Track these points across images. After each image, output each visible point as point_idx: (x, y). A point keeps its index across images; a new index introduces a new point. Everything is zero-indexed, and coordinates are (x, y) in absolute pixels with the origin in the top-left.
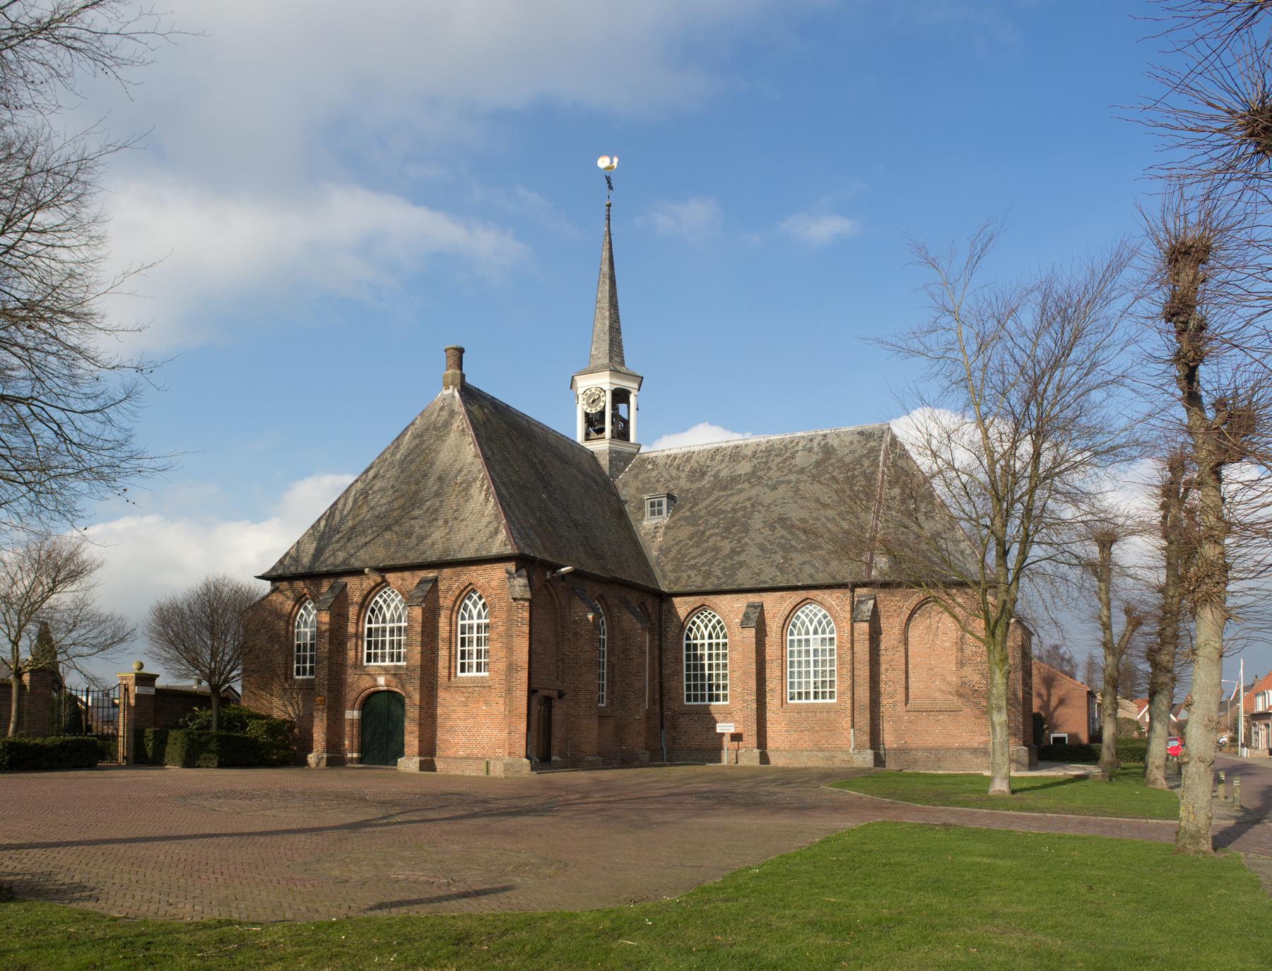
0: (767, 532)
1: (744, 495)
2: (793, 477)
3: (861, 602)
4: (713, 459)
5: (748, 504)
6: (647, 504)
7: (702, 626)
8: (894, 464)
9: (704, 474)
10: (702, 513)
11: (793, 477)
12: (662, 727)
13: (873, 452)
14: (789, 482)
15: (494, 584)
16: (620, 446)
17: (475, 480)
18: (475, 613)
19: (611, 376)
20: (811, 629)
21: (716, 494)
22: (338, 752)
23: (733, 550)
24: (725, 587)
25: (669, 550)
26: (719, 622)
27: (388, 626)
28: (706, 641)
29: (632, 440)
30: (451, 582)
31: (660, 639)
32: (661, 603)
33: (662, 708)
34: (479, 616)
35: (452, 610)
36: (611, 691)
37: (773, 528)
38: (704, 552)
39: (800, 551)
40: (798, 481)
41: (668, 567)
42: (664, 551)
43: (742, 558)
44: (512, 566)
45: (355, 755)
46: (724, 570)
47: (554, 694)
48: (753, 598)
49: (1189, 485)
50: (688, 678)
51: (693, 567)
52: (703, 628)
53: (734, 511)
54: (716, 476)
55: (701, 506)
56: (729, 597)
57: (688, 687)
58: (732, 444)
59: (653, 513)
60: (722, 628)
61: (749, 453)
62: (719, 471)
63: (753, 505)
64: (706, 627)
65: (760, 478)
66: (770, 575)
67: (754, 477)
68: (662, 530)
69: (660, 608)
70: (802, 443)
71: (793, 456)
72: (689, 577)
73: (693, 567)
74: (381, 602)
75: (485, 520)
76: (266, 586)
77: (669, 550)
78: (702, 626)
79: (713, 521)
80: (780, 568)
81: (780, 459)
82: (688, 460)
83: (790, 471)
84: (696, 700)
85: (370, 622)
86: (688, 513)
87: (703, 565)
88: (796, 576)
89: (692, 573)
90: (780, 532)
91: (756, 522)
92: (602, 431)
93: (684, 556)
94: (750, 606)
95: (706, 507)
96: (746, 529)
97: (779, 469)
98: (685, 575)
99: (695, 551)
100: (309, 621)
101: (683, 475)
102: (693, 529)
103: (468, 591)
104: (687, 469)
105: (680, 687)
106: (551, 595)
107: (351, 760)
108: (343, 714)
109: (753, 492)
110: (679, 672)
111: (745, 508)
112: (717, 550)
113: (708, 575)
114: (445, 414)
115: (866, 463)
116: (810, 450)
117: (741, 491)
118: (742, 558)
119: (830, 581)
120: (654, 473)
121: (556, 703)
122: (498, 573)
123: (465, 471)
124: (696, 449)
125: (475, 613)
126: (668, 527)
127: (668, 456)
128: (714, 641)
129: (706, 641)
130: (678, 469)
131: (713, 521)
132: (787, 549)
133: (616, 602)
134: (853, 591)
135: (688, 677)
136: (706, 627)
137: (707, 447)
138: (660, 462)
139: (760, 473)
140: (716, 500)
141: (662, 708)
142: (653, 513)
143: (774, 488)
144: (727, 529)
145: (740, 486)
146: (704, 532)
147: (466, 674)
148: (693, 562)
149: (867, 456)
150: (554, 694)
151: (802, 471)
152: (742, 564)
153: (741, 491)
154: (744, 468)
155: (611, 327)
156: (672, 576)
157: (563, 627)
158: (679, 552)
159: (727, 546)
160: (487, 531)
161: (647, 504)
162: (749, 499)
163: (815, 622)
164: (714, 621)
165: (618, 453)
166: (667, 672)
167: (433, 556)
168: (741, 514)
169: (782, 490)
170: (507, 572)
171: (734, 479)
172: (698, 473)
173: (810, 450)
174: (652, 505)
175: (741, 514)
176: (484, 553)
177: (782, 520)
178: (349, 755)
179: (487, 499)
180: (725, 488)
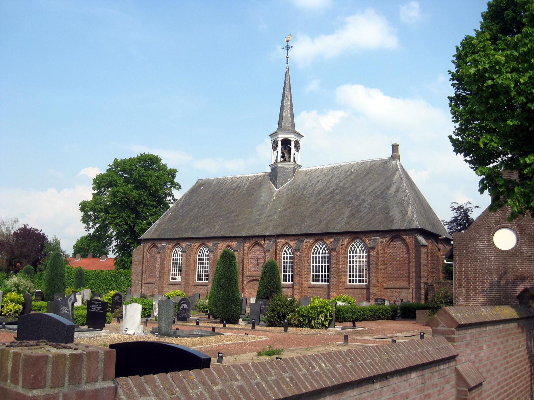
7: (356, 247)
18: (288, 253)
28: (321, 255)
34: (290, 254)
52: (319, 249)
64: (321, 248)
74: (318, 246)
78: (356, 247)
125: (288, 253)
136: (321, 248)
163: (360, 248)
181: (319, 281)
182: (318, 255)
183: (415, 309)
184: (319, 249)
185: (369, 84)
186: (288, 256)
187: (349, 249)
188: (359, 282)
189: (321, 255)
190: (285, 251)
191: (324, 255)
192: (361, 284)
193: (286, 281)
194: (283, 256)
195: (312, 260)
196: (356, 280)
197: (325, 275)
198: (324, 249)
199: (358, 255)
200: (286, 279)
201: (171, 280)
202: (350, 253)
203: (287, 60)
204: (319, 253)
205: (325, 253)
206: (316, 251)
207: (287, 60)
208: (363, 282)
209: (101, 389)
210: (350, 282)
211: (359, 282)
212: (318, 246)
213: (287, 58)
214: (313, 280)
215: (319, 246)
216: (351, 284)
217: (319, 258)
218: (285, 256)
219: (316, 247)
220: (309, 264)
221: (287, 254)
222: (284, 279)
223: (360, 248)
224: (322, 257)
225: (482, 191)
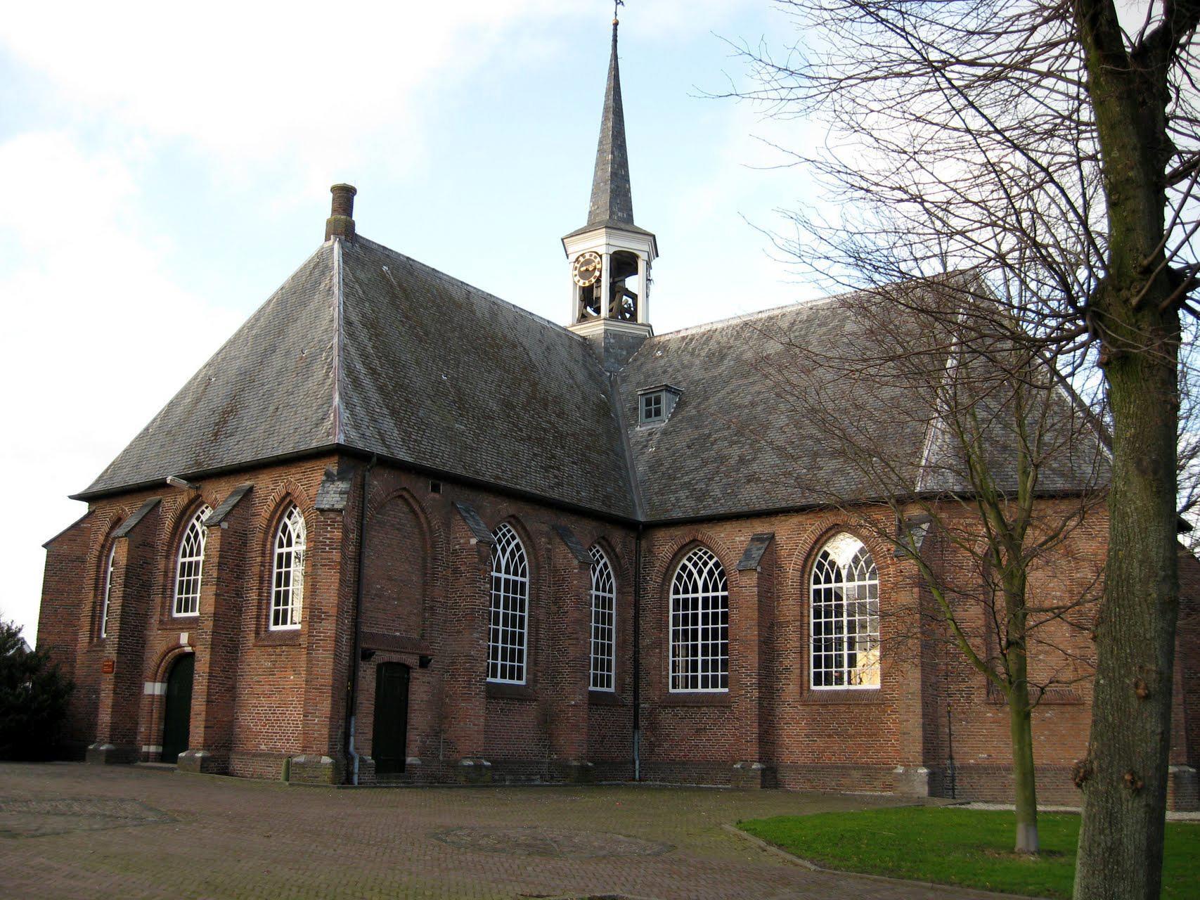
7: (695, 571)
12: (636, 726)
16: (621, 327)
18: (700, 584)
19: (608, 235)
22: (132, 742)
23: (742, 460)
26: (717, 565)
30: (268, 487)
31: (637, 593)
32: (638, 538)
33: (636, 696)
35: (266, 533)
36: (534, 662)
37: (798, 425)
38: (705, 463)
42: (655, 465)
44: (332, 465)
45: (153, 749)
48: (761, 527)
52: (696, 575)
53: (753, 404)
55: (711, 401)
58: (764, 315)
59: (648, 415)
60: (722, 575)
61: (785, 325)
62: (742, 353)
64: (700, 572)
69: (638, 546)
72: (678, 499)
74: (690, 566)
78: (695, 571)
82: (371, 325)
84: (828, 682)
86: (694, 412)
94: (757, 539)
99: (692, 463)
101: (698, 362)
103: (286, 504)
106: (413, 511)
107: (147, 757)
108: (141, 687)
121: (416, 674)
122: (316, 473)
124: (720, 326)
125: (700, 584)
127: (684, 338)
130: (692, 354)
133: (545, 528)
136: (700, 572)
137: (734, 322)
138: (673, 346)
141: (636, 696)
142: (648, 415)
144: (739, 433)
146: (710, 435)
147: (280, 628)
148: (686, 479)
150: (412, 660)
155: (614, 174)
157: (435, 559)
159: (735, 452)
163: (705, 574)
164: (711, 564)
165: (616, 336)
166: (645, 642)
172: (720, 355)
174: (648, 403)
178: (145, 749)
182: (690, 596)
184: (696, 575)
187: (674, 580)
188: (705, 685)
189: (700, 595)
191: (711, 594)
193: (695, 686)
195: (671, 628)
197: (715, 662)
199: (700, 595)
200: (695, 678)
202: (677, 592)
203: (615, 30)
207: (615, 30)
211: (705, 685)
212: (690, 566)
213: (616, 24)
215: (695, 565)
216: (823, 688)
217: (695, 607)
219: (684, 568)
220: (662, 626)
222: (818, 675)
223: (705, 574)
225: (44, 546)
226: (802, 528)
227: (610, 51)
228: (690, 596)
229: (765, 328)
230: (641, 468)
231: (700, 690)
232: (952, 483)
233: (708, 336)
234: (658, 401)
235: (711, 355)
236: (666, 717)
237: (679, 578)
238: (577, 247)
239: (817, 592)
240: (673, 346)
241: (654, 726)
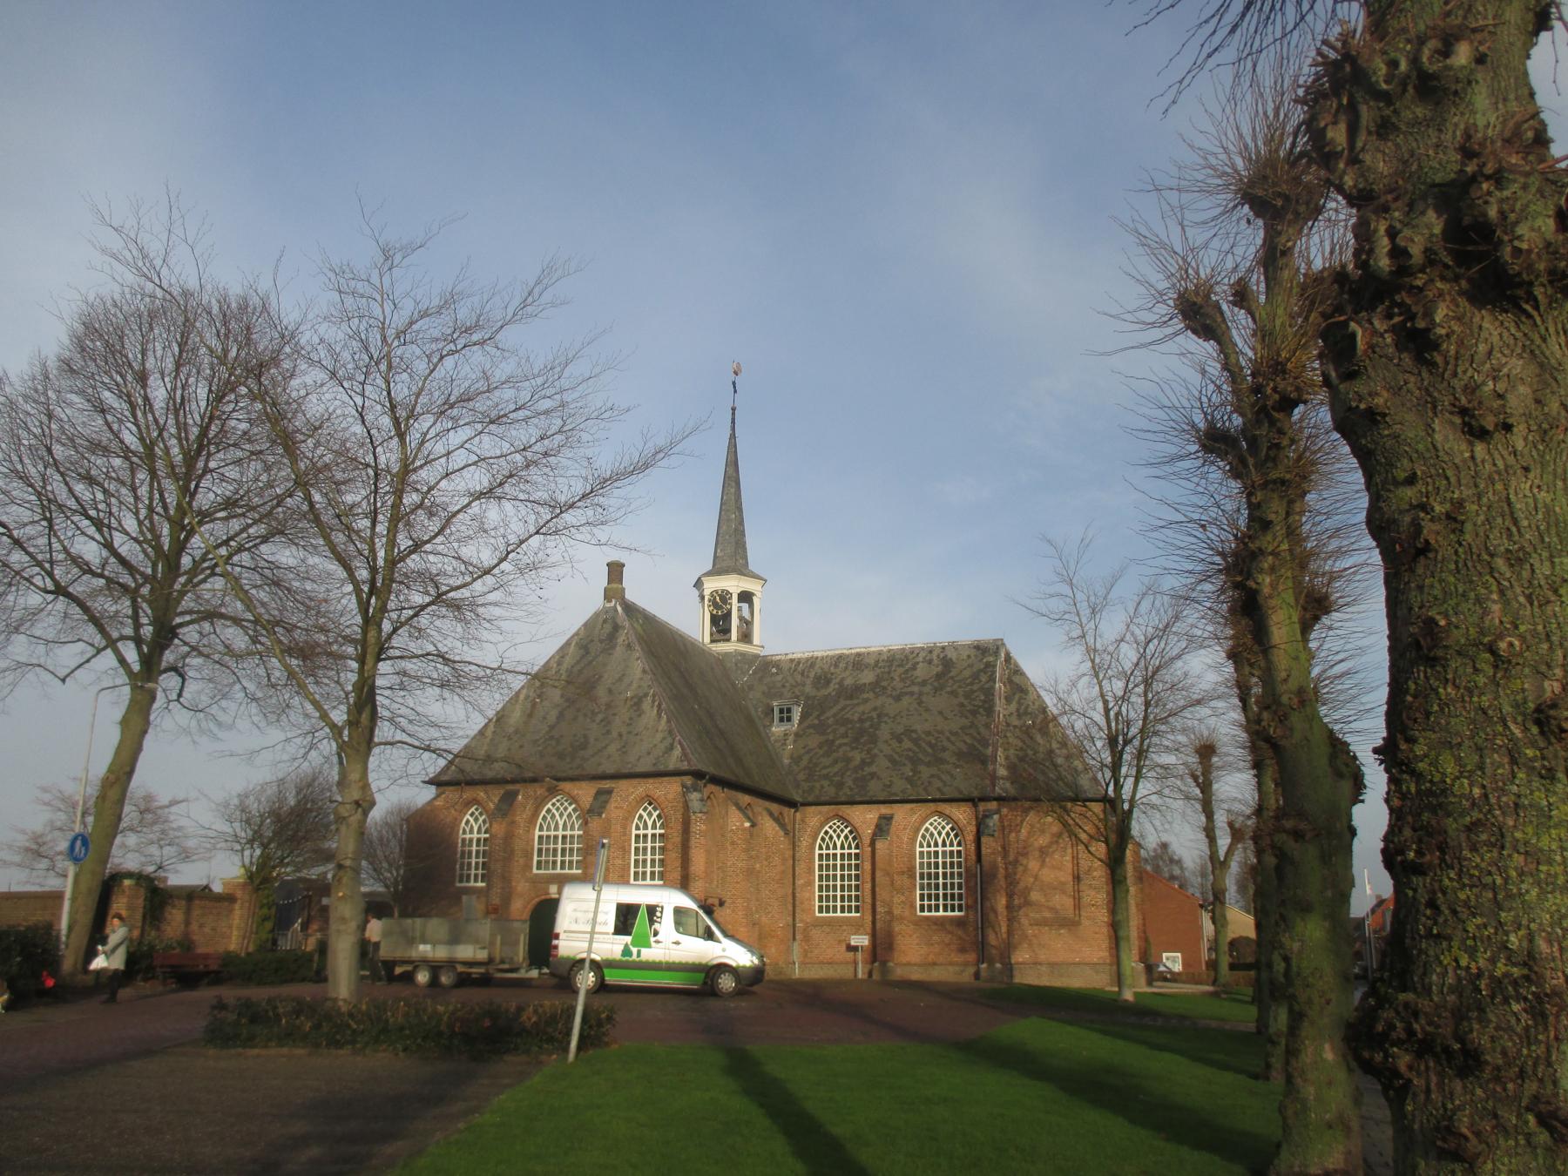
0: (895, 744)
1: (868, 707)
2: (916, 689)
3: (986, 816)
4: (836, 666)
5: (874, 714)
6: (776, 711)
8: (1010, 681)
9: (828, 682)
10: (830, 721)
11: (916, 689)
13: (990, 667)
14: (912, 694)
15: (670, 796)
17: (646, 695)
18: (650, 824)
20: (940, 842)
21: (842, 703)
23: (863, 761)
24: (858, 798)
25: (800, 758)
27: (560, 833)
28: (839, 851)
29: (756, 640)
34: (654, 827)
37: (900, 741)
38: (836, 762)
39: (928, 764)
40: (921, 694)
41: (801, 776)
42: (796, 759)
43: (873, 769)
44: (688, 780)
46: (856, 780)
47: (716, 902)
49: (1299, 315)
50: (821, 889)
51: (826, 777)
53: (861, 720)
54: (841, 683)
55: (829, 714)
56: (861, 807)
57: (821, 897)
59: (781, 720)
63: (879, 716)
64: (561, 815)
65: (884, 688)
66: (900, 786)
67: (877, 687)
68: (791, 738)
70: (922, 654)
71: (914, 668)
73: (826, 777)
75: (659, 736)
76: (431, 792)
77: (800, 758)
79: (842, 730)
80: (909, 780)
81: (901, 670)
82: (812, 665)
83: (913, 683)
85: (638, 828)
87: (836, 774)
88: (925, 789)
89: (826, 783)
90: (907, 744)
91: (884, 732)
92: (728, 631)
93: (816, 765)
95: (834, 716)
96: (874, 740)
97: (902, 680)
98: (818, 785)
99: (826, 761)
100: (472, 827)
101: (808, 682)
102: (822, 739)
104: (812, 675)
105: (811, 899)
107: (363, 928)
109: (878, 703)
110: (811, 883)
111: (871, 718)
112: (848, 760)
113: (840, 785)
114: (608, 628)
115: (984, 678)
116: (930, 662)
117: (866, 701)
118: (873, 769)
119: (957, 795)
120: (779, 678)
123: (635, 685)
125: (650, 824)
126: (797, 735)
128: (948, 849)
129: (940, 849)
131: (842, 730)
132: (915, 761)
134: (975, 806)
135: (821, 887)
136: (940, 834)
138: (785, 667)
139: (884, 684)
140: (843, 709)
143: (898, 699)
144: (856, 740)
145: (865, 696)
148: (825, 772)
149: (983, 671)
151: (924, 683)
152: (873, 775)
153: (866, 701)
154: (868, 677)
156: (805, 786)
158: (810, 761)
159: (857, 757)
160: (662, 746)
161: (776, 711)
162: (875, 709)
166: (799, 882)
167: (610, 768)
168: (867, 724)
169: (906, 701)
170: (683, 786)
171: (858, 689)
172: (823, 680)
173: (930, 662)
174: (781, 711)
175: (867, 724)
176: (662, 768)
177: (908, 732)
179: (659, 715)
180: (851, 698)
181: (937, 910)
183: (171, 896)
185: (1265, 240)
186: (650, 832)
190: (641, 817)
192: (949, 913)
194: (634, 832)
195: (633, 858)
196: (835, 908)
198: (846, 837)
201: (535, 871)
204: (835, 847)
205: (952, 845)
206: (828, 841)
208: (953, 910)
209: (1333, 410)
210: (821, 911)
211: (843, 911)
213: (734, 409)
214: (821, 908)
218: (641, 832)
219: (549, 811)
220: (811, 871)
221: (646, 827)
224: (944, 853)
226: (913, 811)
227: (729, 432)
228: (552, 833)
229: (857, 662)
230: (786, 761)
231: (839, 914)
232: (1012, 791)
233: (812, 662)
234: (789, 710)
235: (818, 678)
236: (816, 933)
237: (544, 818)
238: (711, 585)
239: (637, 836)
240: (785, 667)
241: (807, 939)
